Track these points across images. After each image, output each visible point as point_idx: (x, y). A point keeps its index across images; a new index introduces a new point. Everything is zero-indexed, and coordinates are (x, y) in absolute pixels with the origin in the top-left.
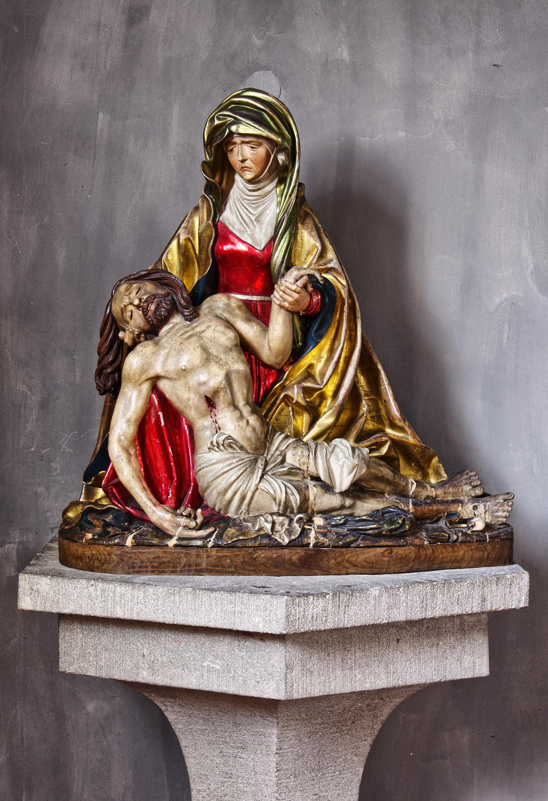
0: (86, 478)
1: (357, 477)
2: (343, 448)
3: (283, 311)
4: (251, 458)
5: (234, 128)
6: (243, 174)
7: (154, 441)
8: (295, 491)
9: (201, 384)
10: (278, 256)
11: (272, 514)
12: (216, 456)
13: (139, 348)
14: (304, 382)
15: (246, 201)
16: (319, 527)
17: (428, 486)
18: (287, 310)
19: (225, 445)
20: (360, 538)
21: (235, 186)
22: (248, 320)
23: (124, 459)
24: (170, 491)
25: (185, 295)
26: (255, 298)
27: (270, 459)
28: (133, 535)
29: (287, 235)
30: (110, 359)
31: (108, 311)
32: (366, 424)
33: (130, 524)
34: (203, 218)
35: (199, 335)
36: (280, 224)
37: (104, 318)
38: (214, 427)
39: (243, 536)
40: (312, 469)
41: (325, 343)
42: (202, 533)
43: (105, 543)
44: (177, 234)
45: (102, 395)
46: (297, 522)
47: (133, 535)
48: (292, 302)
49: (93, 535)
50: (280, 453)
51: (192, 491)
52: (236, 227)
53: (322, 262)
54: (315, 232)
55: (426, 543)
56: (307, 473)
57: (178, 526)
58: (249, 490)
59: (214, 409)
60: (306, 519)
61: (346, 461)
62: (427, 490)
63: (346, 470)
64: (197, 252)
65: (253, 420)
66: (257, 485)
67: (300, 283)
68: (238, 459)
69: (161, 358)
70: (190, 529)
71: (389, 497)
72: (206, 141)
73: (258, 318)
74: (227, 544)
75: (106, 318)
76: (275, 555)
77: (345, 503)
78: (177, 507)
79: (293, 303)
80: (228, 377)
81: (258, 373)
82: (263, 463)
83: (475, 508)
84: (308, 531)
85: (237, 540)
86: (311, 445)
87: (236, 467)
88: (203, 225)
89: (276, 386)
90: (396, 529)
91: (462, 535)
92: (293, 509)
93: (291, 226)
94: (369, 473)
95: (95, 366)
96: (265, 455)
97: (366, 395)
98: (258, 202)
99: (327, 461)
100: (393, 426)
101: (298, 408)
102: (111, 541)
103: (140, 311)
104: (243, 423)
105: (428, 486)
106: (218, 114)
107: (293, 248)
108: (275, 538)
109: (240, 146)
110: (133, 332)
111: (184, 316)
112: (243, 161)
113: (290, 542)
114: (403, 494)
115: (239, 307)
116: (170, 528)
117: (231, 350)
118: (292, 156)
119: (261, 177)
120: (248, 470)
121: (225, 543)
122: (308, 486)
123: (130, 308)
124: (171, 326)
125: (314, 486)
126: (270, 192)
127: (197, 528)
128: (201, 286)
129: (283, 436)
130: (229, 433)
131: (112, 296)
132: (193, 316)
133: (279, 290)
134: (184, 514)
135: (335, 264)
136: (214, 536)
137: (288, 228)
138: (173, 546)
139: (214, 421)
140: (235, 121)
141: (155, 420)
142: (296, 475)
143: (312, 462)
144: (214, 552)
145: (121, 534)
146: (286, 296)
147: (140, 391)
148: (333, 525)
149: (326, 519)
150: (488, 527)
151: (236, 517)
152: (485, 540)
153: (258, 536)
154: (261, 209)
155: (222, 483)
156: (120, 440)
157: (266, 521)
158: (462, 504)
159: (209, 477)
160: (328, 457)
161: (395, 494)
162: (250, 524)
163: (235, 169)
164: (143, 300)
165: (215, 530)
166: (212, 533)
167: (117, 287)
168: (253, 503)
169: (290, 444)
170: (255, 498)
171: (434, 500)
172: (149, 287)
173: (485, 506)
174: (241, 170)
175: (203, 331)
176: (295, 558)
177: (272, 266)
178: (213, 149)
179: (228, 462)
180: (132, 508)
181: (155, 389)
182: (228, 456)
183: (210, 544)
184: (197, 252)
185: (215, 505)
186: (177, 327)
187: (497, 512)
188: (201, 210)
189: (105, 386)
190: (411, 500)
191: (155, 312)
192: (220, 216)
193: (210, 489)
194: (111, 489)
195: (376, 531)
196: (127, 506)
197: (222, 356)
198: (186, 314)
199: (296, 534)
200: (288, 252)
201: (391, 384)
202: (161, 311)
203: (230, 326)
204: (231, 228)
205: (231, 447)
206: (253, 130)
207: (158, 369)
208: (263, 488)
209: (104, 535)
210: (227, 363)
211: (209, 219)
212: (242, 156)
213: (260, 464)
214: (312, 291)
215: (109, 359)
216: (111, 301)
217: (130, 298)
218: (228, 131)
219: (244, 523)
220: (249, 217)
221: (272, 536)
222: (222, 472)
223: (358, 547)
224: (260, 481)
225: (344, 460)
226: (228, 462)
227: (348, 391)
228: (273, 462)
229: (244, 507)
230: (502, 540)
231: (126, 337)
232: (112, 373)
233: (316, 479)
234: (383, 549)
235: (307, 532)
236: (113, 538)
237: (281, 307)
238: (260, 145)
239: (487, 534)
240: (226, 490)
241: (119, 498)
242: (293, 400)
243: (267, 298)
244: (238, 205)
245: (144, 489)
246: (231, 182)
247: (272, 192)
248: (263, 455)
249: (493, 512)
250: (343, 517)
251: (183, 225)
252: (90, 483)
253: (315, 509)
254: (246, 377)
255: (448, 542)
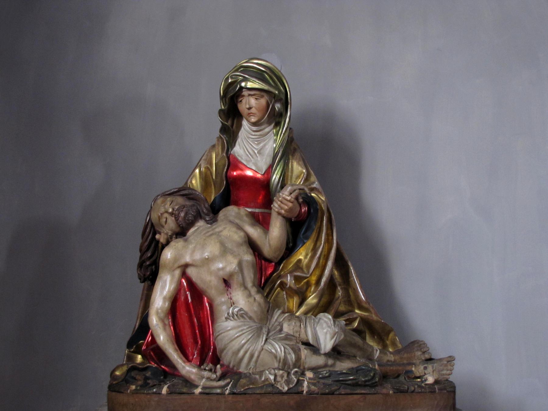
0: (129, 345)
1: (337, 341)
2: (326, 320)
3: (280, 217)
4: (258, 326)
5: (243, 84)
6: (249, 119)
7: (183, 315)
8: (291, 352)
9: (219, 269)
10: (276, 177)
11: (274, 369)
12: (230, 324)
13: (172, 244)
14: (295, 272)
15: (251, 139)
16: (310, 379)
17: (388, 353)
18: (284, 217)
19: (238, 315)
20: (342, 387)
21: (242, 129)
22: (253, 225)
23: (161, 327)
24: (196, 353)
25: (207, 206)
26: (257, 210)
27: (271, 328)
28: (168, 385)
29: (282, 163)
30: (149, 255)
31: (148, 218)
32: (340, 307)
33: (165, 377)
34: (218, 153)
35: (218, 234)
36: (277, 154)
37: (145, 223)
38: (230, 302)
39: (253, 385)
40: (303, 336)
41: (309, 244)
42: (222, 383)
43: (145, 392)
44: (199, 164)
45: (142, 282)
46: (294, 374)
47: (168, 385)
48: (287, 209)
49: (136, 387)
50: (278, 324)
51: (212, 353)
52: (243, 158)
53: (307, 183)
54: (302, 162)
55: (391, 392)
56: (299, 339)
57: (203, 377)
58: (256, 350)
59: (230, 289)
60: (300, 372)
61: (329, 329)
62: (388, 355)
63: (328, 336)
64: (214, 177)
65: (258, 297)
66: (262, 347)
67: (293, 195)
68: (248, 327)
69: (189, 252)
70: (211, 380)
71: (360, 359)
72: (222, 95)
73: (260, 223)
74: (240, 391)
75: (146, 223)
76: (277, 400)
77: (328, 362)
78: (202, 362)
79: (288, 210)
80: (240, 264)
81: (260, 265)
82: (267, 330)
83: (425, 368)
84: (302, 381)
85: (248, 388)
86: (302, 317)
87: (246, 332)
88: (219, 157)
89: (274, 275)
90: (369, 381)
91: (418, 387)
92: (290, 366)
93: (285, 156)
94: (344, 340)
95: (137, 261)
96: (268, 325)
97: (340, 285)
98: (260, 140)
99: (315, 329)
100: (361, 308)
101: (292, 292)
102: (150, 390)
103: (173, 217)
104: (251, 300)
105: (388, 353)
106: (232, 74)
107: (286, 173)
108: (277, 386)
109: (247, 98)
110: (167, 234)
111: (206, 221)
112: (250, 108)
113: (288, 390)
114: (370, 358)
115: (247, 215)
116: (196, 380)
117: (241, 245)
118: (286, 104)
119: (262, 121)
120: (256, 334)
121: (239, 391)
122: (300, 349)
123: (166, 215)
124: (196, 228)
125: (305, 348)
126: (269, 132)
127: (217, 379)
128: (217, 201)
129: (280, 311)
130: (241, 306)
131: (151, 207)
132: (213, 220)
133: (277, 201)
134: (207, 368)
135: (316, 185)
136: (230, 386)
137: (282, 159)
138: (199, 393)
139: (230, 298)
140: (245, 79)
141: (184, 298)
142: (290, 340)
143: (303, 331)
144: (230, 398)
145: (159, 385)
146: (282, 205)
147: (173, 276)
148: (320, 377)
149: (315, 373)
150: (436, 382)
151: (246, 372)
152: (435, 392)
153: (264, 386)
154: (261, 145)
155: (235, 345)
156: (157, 313)
157: (270, 373)
158: (415, 366)
159: (226, 341)
160: (315, 326)
161: (363, 357)
162: (257, 376)
163: (243, 114)
164: (175, 209)
165: (231, 381)
166: (227, 384)
167: (155, 200)
168: (259, 360)
169: (285, 317)
170: (261, 356)
171: (394, 363)
172: (180, 200)
173: (433, 367)
174: (248, 115)
175: (221, 231)
176: (292, 403)
177: (271, 186)
178: (227, 100)
179: (240, 329)
180: (166, 366)
181: (184, 274)
182: (240, 324)
183: (227, 392)
184: (214, 177)
185: (230, 363)
186: (201, 229)
187: (442, 370)
188: (217, 147)
189: (144, 275)
190: (376, 363)
191: (185, 217)
192: (231, 150)
193: (227, 349)
194: (150, 352)
195: (354, 381)
196: (162, 365)
197: (235, 249)
198: (207, 219)
199: (293, 383)
200: (282, 175)
201: (357, 276)
202: (189, 217)
203: (240, 228)
204: (239, 159)
205: (243, 317)
206: (258, 86)
207: (188, 259)
208: (267, 348)
209: (145, 385)
210: (239, 255)
211: (224, 152)
212: (249, 104)
213: (265, 330)
214: (302, 202)
215: (148, 255)
216: (150, 211)
217: (165, 208)
218: (239, 86)
219: (253, 376)
220: (253, 150)
221: (275, 385)
222: (236, 336)
223: (340, 394)
224: (265, 344)
225: (327, 328)
226: (240, 329)
227: (327, 279)
228: (274, 330)
229: (252, 364)
230: (448, 392)
231: (161, 238)
232: (150, 265)
233: (307, 344)
234: (359, 396)
235: (301, 383)
236: (152, 388)
237: (279, 214)
238: (262, 97)
239: (436, 387)
240: (239, 350)
241: (155, 359)
242: (287, 285)
243: (266, 211)
244: (244, 142)
245: (176, 349)
246: (240, 126)
247: (270, 133)
248: (266, 325)
249: (439, 371)
250: (328, 371)
251: (203, 158)
252: (132, 350)
253: (306, 366)
254: (253, 266)
255: (407, 392)
